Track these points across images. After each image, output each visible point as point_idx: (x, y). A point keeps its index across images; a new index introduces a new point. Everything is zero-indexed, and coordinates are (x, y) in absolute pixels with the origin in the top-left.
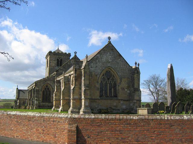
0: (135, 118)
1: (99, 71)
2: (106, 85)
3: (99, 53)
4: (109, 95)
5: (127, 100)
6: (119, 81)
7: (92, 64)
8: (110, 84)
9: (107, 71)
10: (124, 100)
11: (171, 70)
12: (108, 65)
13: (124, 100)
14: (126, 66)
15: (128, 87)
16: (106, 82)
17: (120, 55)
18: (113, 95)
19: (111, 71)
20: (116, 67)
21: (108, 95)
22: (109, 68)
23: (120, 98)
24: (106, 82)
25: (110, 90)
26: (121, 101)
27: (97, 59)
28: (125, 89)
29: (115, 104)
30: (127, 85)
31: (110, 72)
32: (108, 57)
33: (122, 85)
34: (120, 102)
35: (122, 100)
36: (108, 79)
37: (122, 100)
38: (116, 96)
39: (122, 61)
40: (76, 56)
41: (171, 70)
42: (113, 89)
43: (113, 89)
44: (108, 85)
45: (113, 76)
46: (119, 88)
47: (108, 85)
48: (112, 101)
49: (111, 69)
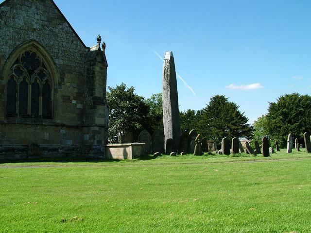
2: (24, 84)
6: (57, 78)
8: (35, 85)
9: (27, 53)
10: (69, 127)
14: (77, 45)
16: (24, 79)
18: (41, 113)
19: (38, 54)
21: (29, 113)
22: (33, 45)
25: (35, 101)
26: (60, 128)
28: (72, 98)
29: (46, 135)
30: (76, 91)
33: (66, 88)
36: (31, 72)
37: (63, 126)
38: (49, 115)
39: (67, 32)
43: (41, 98)
44: (30, 86)
45: (44, 66)
46: (57, 96)
47: (30, 86)
49: (37, 48)
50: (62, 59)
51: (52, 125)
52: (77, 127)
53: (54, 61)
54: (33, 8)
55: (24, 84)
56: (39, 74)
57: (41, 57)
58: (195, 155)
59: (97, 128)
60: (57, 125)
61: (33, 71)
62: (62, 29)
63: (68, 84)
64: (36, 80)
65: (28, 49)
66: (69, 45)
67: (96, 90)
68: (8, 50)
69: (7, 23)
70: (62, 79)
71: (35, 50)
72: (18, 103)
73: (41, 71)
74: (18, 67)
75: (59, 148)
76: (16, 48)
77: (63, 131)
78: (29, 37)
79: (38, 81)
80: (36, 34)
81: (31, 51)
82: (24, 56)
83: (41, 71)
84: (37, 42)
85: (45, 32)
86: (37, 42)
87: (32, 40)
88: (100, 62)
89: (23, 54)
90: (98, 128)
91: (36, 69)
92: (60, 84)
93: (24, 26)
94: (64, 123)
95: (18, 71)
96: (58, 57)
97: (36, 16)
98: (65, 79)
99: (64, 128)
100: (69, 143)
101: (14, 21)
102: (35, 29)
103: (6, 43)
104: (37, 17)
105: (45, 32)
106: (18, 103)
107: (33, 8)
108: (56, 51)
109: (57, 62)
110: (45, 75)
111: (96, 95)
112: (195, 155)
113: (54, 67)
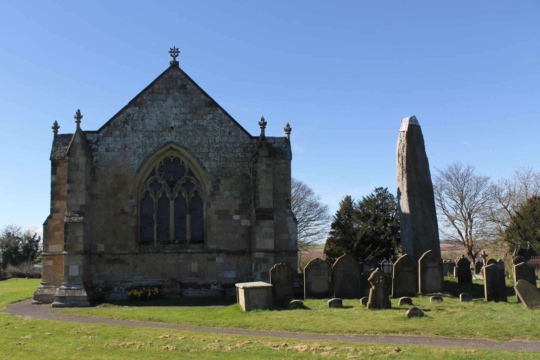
0: (41, 241)
1: (135, 162)
2: (164, 200)
3: (133, 103)
4: (176, 238)
5: (242, 253)
6: (208, 188)
7: (110, 140)
8: (179, 200)
9: (167, 160)
10: (229, 253)
11: (414, 136)
12: (168, 139)
13: (229, 253)
14: (237, 136)
15: (243, 210)
16: (164, 194)
17: (213, 104)
18: (188, 237)
19: (182, 159)
20: (197, 141)
21: (172, 238)
22: (171, 148)
23: (212, 246)
24: (164, 194)
25: (180, 219)
26: (215, 255)
27: (126, 122)
28: (232, 212)
29: (194, 267)
30: (238, 201)
31: (177, 160)
32: (171, 111)
33: (220, 203)
34: (214, 260)
35: (219, 252)
36: (172, 184)
37: (219, 252)
38: (199, 240)
39: (221, 122)
40: (175, 65)
41: (414, 136)
42: (188, 216)
43: (188, 216)
44: (172, 203)
45: (190, 173)
46: (209, 212)
47: (172, 203)
48: (182, 256)
49: (178, 151)
50: (214, 160)
51: (204, 252)
52: (242, 253)
53: (201, 165)
54: (170, 101)
55: (164, 200)
56: (183, 185)
57: (186, 162)
58: (370, 308)
59: (261, 255)
60: (211, 252)
61: (175, 182)
62: (213, 119)
63: (226, 194)
64: (180, 193)
65: (168, 155)
66: (225, 139)
67: (261, 198)
68: (136, 161)
69: (135, 128)
70: (216, 187)
71: (176, 155)
72: (155, 226)
73: (188, 180)
74: (155, 180)
75: (213, 283)
76: (148, 157)
77: (220, 260)
78: (165, 139)
79: (183, 194)
80: (174, 133)
81: (172, 157)
82: (163, 164)
83: (188, 180)
84: (176, 144)
85: (188, 128)
86: (176, 144)
87: (168, 143)
88: (265, 157)
89: (161, 163)
90: (263, 253)
91: (180, 178)
92: (213, 195)
93: (158, 127)
94: (222, 248)
95: (155, 184)
96: (208, 159)
97: (174, 109)
98: (220, 187)
99: (222, 254)
100: (229, 276)
101: (144, 123)
102: (172, 128)
103: (135, 153)
104: (175, 111)
105: (188, 128)
106: (155, 226)
107: (170, 101)
108: (205, 150)
109: (207, 165)
110: (193, 185)
111: (260, 206)
112: (370, 308)
113: (202, 173)
